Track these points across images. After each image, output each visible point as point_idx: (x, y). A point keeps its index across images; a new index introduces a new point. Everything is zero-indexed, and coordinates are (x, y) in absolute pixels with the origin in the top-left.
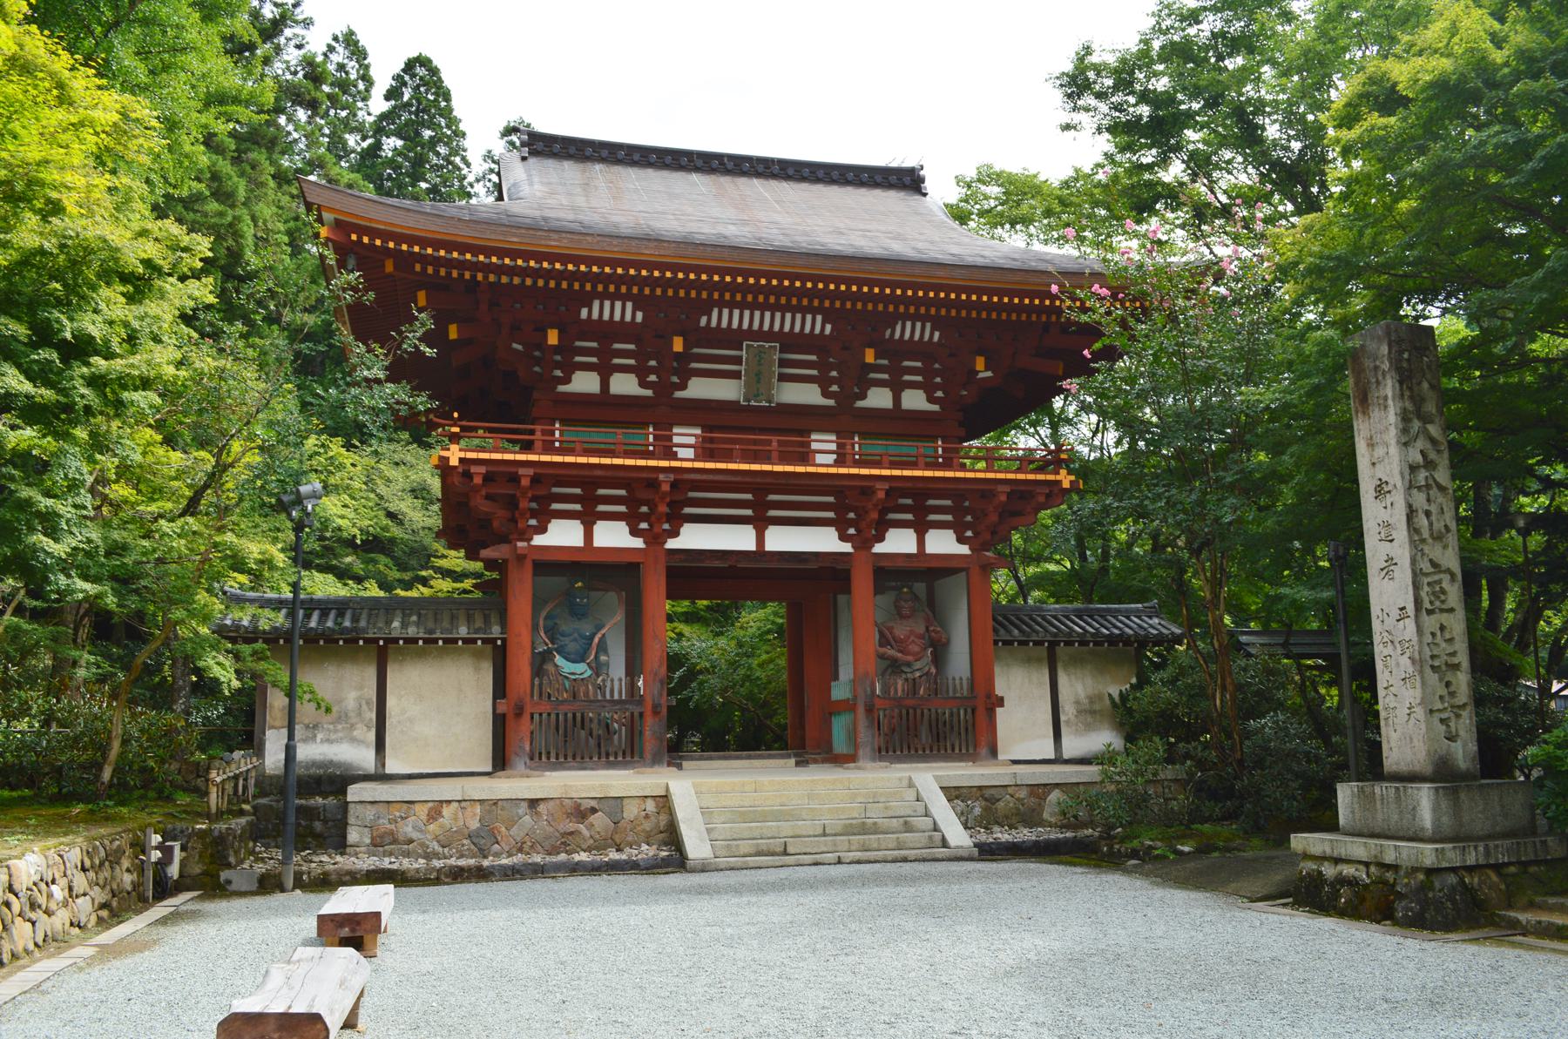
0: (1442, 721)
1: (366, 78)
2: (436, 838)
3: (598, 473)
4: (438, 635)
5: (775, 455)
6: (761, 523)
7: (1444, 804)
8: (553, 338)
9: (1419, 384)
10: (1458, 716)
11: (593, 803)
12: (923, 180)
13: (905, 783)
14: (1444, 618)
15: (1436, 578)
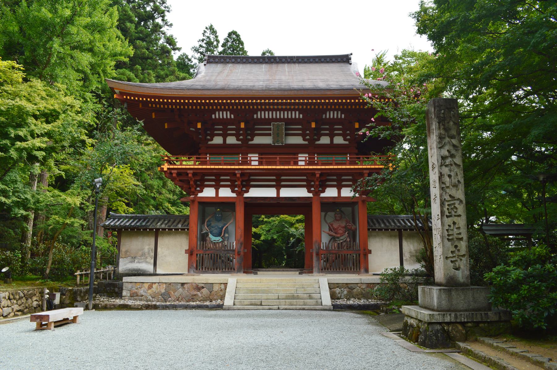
0: (452, 262)
1: (218, 41)
2: (150, 295)
3: (215, 171)
4: (172, 227)
5: (278, 162)
6: (278, 187)
7: (443, 296)
8: (313, 125)
9: (448, 123)
10: (461, 260)
11: (203, 285)
12: (350, 59)
13: (317, 281)
14: (455, 219)
15: (452, 202)
